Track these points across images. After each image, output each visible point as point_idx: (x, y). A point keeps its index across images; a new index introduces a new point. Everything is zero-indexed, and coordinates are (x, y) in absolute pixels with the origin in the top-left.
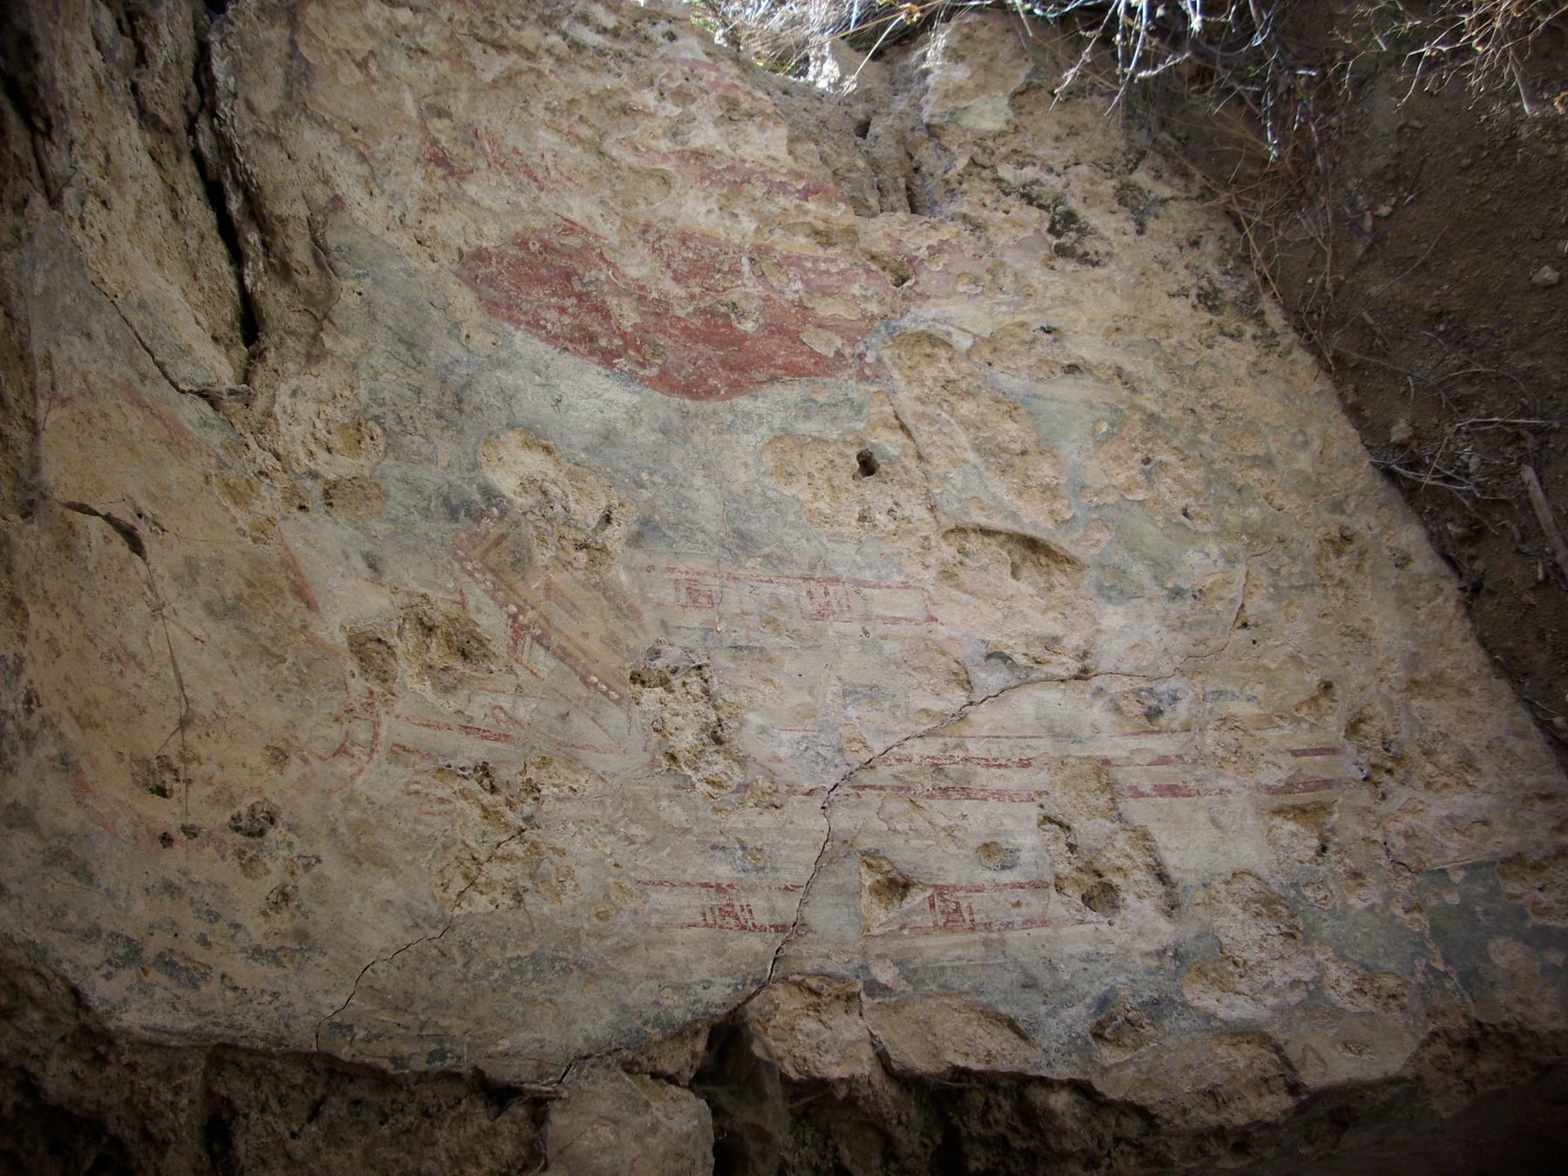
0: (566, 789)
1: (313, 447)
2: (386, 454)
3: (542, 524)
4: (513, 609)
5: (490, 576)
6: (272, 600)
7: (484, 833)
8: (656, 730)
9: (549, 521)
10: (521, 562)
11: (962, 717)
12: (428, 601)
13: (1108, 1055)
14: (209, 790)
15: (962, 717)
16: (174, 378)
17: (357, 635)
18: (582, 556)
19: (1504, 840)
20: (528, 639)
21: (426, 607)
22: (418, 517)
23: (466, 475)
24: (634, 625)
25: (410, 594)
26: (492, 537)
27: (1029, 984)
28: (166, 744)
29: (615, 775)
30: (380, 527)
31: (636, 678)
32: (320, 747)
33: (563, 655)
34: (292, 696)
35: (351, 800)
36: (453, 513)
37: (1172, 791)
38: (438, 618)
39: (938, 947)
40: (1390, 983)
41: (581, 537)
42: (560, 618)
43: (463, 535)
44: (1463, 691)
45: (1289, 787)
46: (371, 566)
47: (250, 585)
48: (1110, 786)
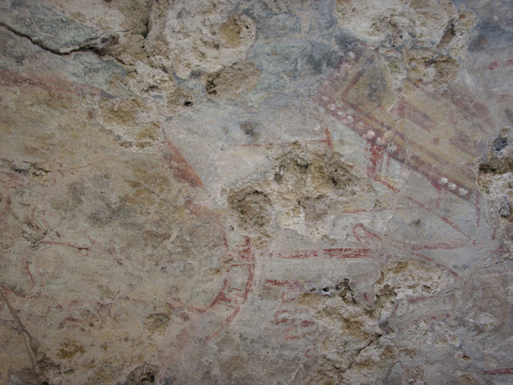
0: (419, 288)
1: (203, 49)
2: (257, 37)
3: (393, 54)
4: (371, 134)
5: (351, 111)
6: (157, 191)
7: (346, 343)
8: (503, 216)
9: (399, 50)
10: (376, 91)
12: (299, 146)
14: (90, 372)
16: (54, 47)
17: (237, 194)
18: (431, 71)
20: (386, 157)
21: (298, 152)
22: (287, 79)
23: (325, 32)
24: (480, 121)
25: (282, 146)
26: (350, 78)
29: (465, 267)
30: (255, 98)
31: (484, 169)
32: (200, 302)
33: (417, 165)
34: (175, 265)
35: (226, 341)
36: (317, 67)
38: (310, 158)
41: (428, 55)
42: (414, 131)
43: (326, 83)
46: (248, 132)
47: (135, 185)
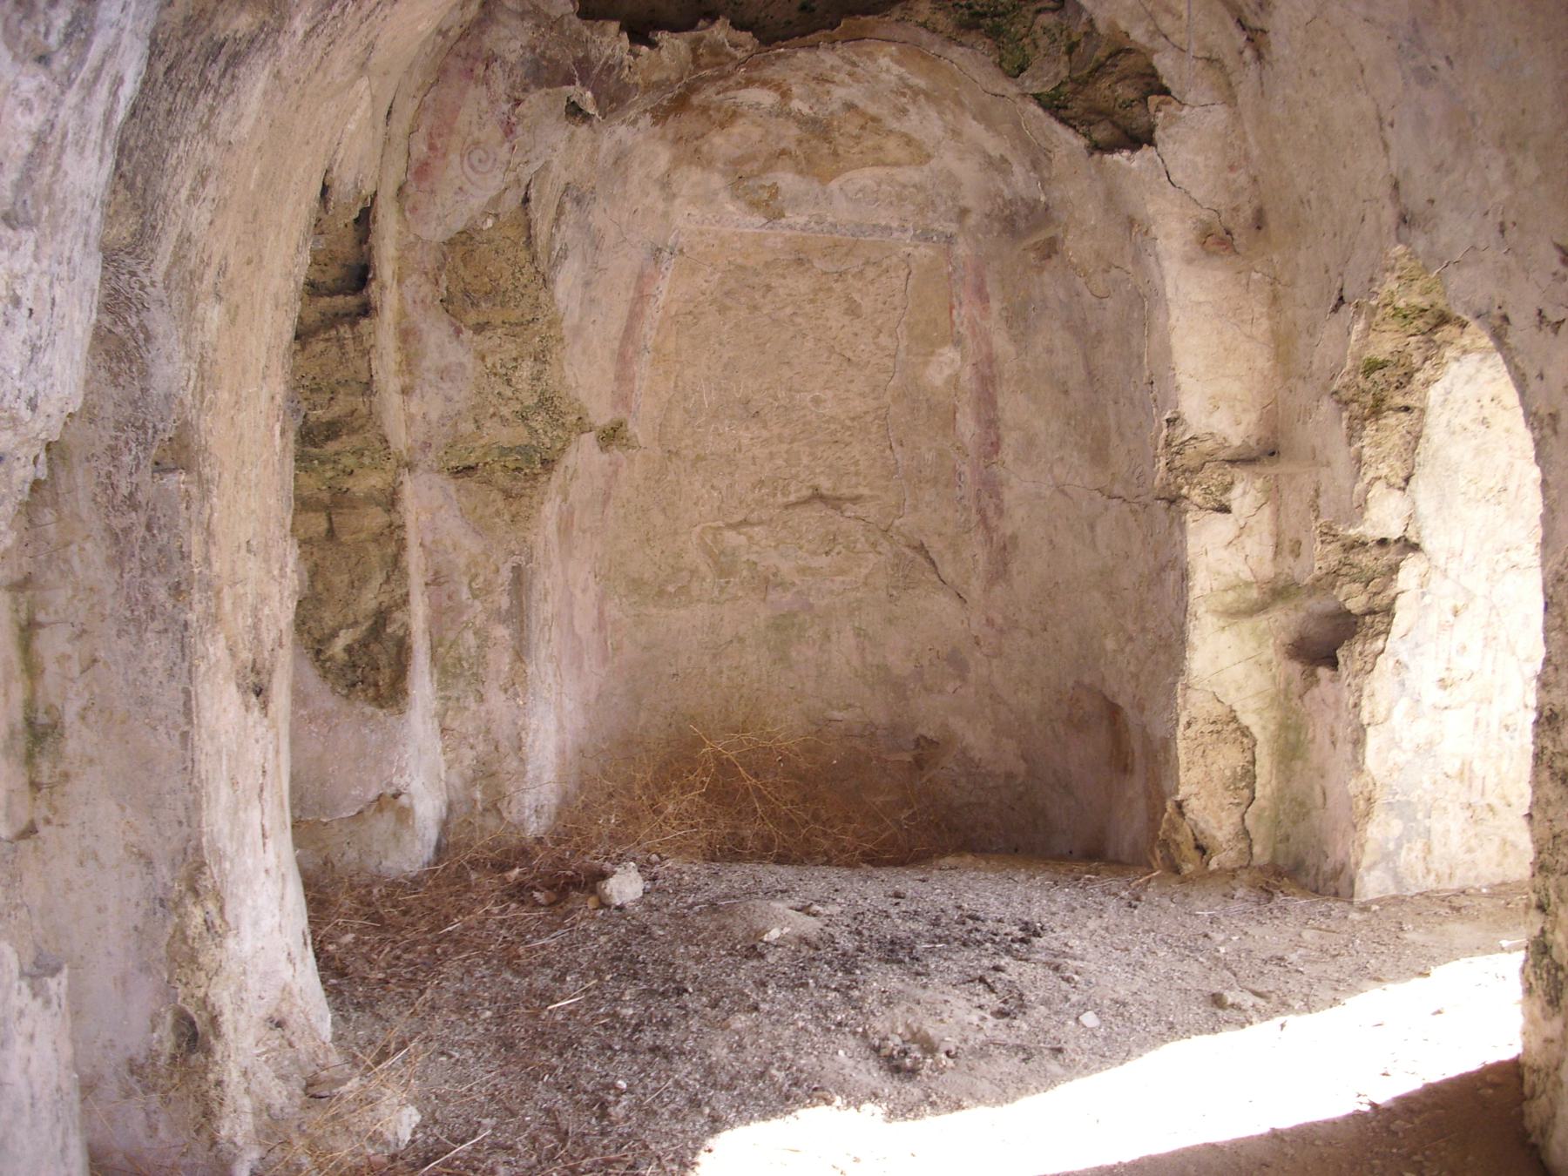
11: (1513, 654)
13: (1391, 663)
15: (1513, 654)
19: (1438, 850)
27: (1417, 645)
28: (20, 566)
37: (1477, 724)
39: (1433, 619)
40: (1395, 776)
44: (1499, 865)
45: (1471, 770)
48: (1482, 701)
